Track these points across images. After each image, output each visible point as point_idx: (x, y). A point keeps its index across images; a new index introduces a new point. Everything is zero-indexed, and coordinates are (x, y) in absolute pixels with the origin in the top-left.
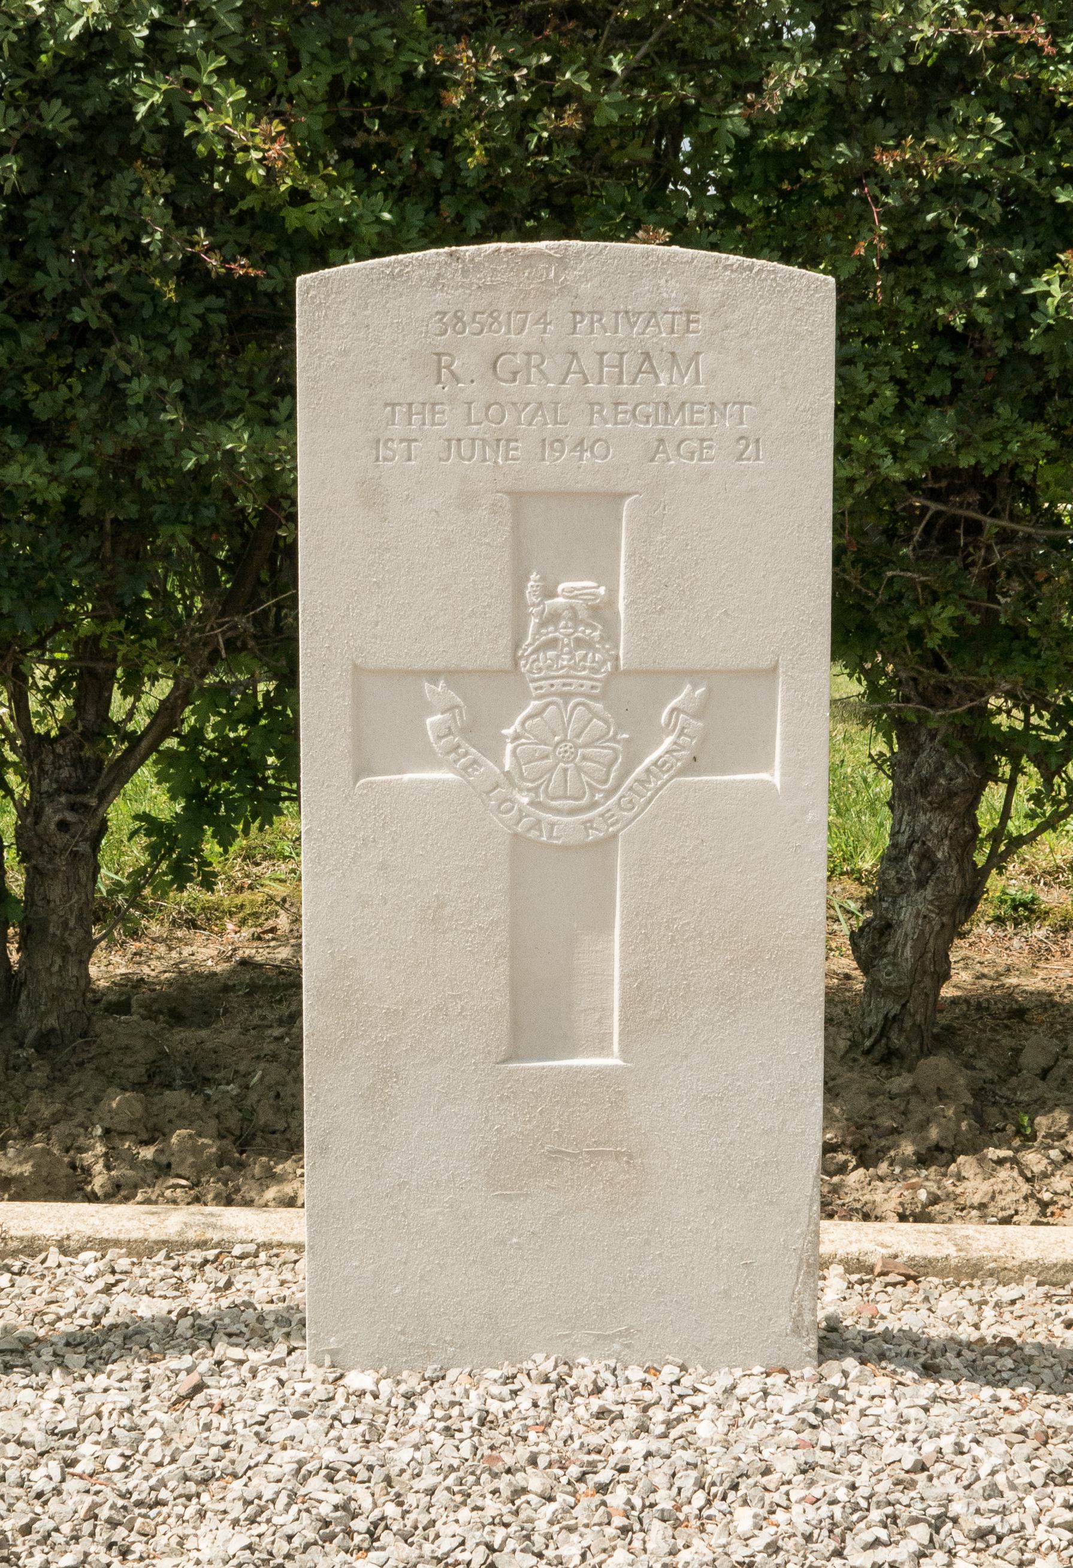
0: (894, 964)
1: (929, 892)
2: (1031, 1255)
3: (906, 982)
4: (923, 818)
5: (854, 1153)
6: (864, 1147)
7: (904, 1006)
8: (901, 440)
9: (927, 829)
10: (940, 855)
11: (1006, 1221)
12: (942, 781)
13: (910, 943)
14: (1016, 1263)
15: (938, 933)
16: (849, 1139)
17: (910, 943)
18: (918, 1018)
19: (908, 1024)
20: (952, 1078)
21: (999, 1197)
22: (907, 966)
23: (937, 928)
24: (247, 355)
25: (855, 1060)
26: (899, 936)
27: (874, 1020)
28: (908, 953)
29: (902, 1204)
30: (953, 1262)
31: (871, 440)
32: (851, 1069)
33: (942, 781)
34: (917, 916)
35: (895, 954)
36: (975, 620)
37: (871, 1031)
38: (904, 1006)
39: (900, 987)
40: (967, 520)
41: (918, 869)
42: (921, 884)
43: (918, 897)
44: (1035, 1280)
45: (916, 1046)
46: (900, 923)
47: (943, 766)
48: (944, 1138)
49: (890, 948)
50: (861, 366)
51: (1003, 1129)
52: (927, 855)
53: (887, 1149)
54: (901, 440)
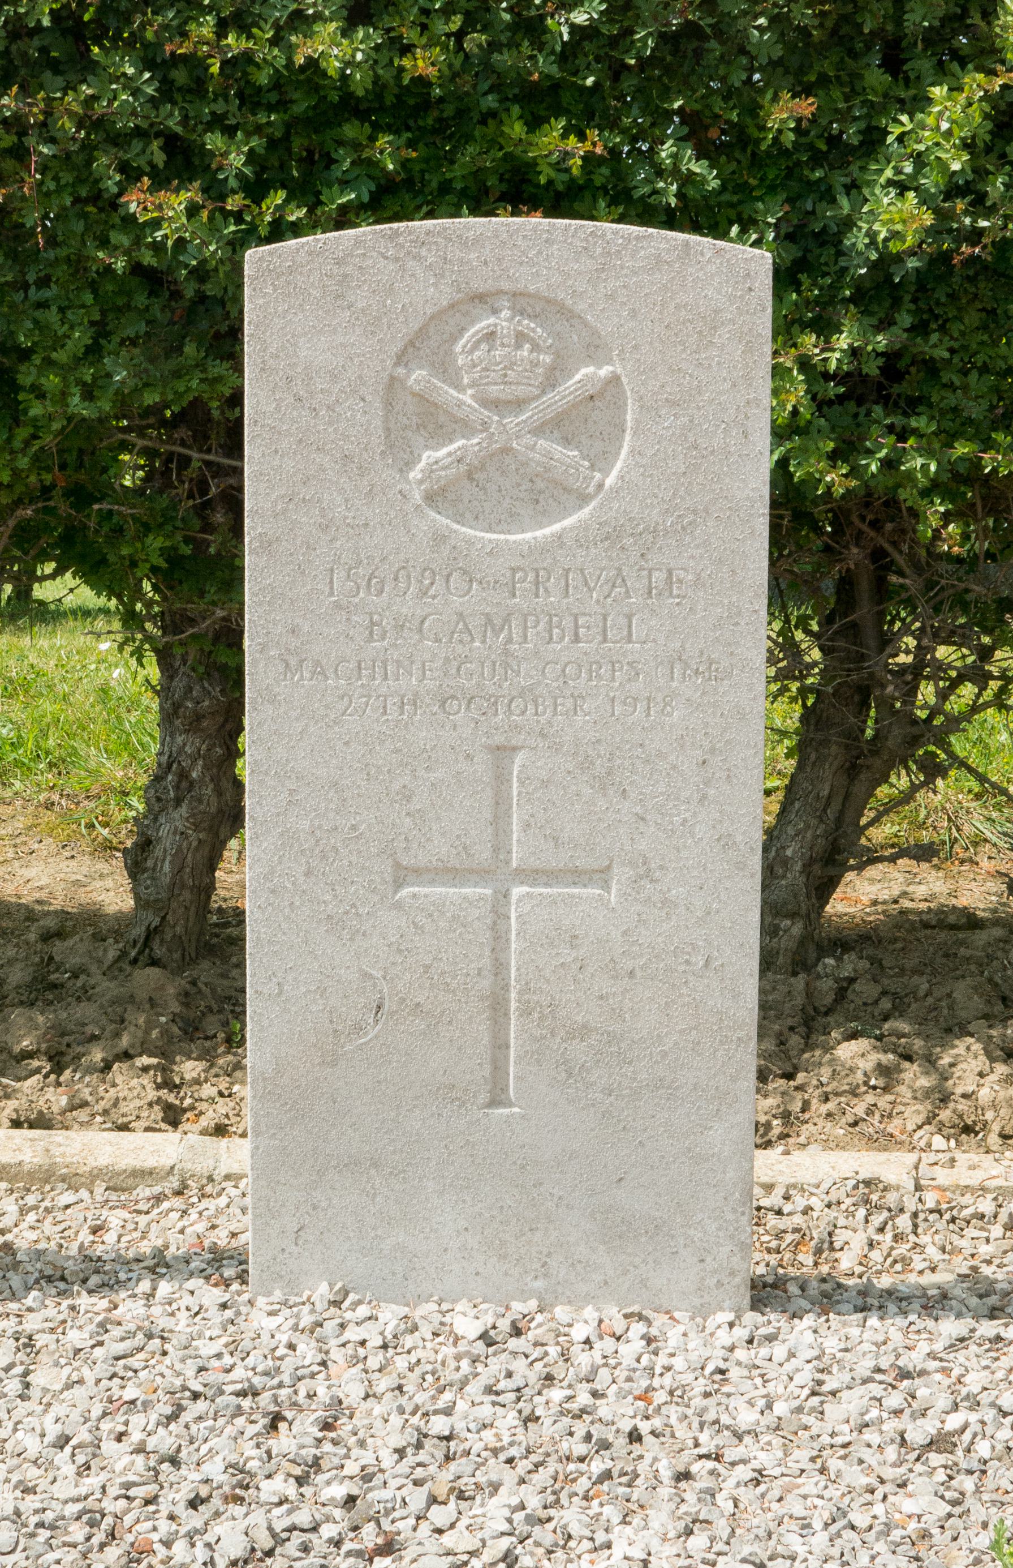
0: (153, 879)
1: (184, 810)
2: (103, 1161)
3: (163, 895)
4: (179, 740)
5: (50, 1059)
6: (62, 1054)
7: (164, 918)
8: (88, 379)
9: (181, 750)
10: (194, 775)
11: (124, 1128)
12: (189, 705)
13: (168, 858)
14: (87, 1169)
15: (197, 849)
16: (44, 1046)
17: (168, 858)
18: (178, 929)
19: (168, 936)
20: (162, 988)
21: (122, 1104)
22: (166, 880)
23: (195, 844)
24: (202, 316)
25: (121, 970)
26: (158, 852)
27: (138, 932)
28: (167, 867)
29: (16, 1110)
30: (26, 1168)
31: (64, 379)
32: (110, 980)
33: (189, 705)
34: (175, 833)
35: (154, 869)
36: (187, 550)
37: (135, 942)
38: (164, 918)
39: (156, 901)
40: (180, 455)
41: (177, 788)
42: (178, 802)
43: (175, 815)
44: (104, 1185)
45: (177, 956)
46: (159, 840)
47: (191, 690)
48: (132, 1046)
49: (150, 863)
50: (54, 309)
51: (215, 1036)
52: (183, 775)
53: (78, 1057)
54: (88, 379)
